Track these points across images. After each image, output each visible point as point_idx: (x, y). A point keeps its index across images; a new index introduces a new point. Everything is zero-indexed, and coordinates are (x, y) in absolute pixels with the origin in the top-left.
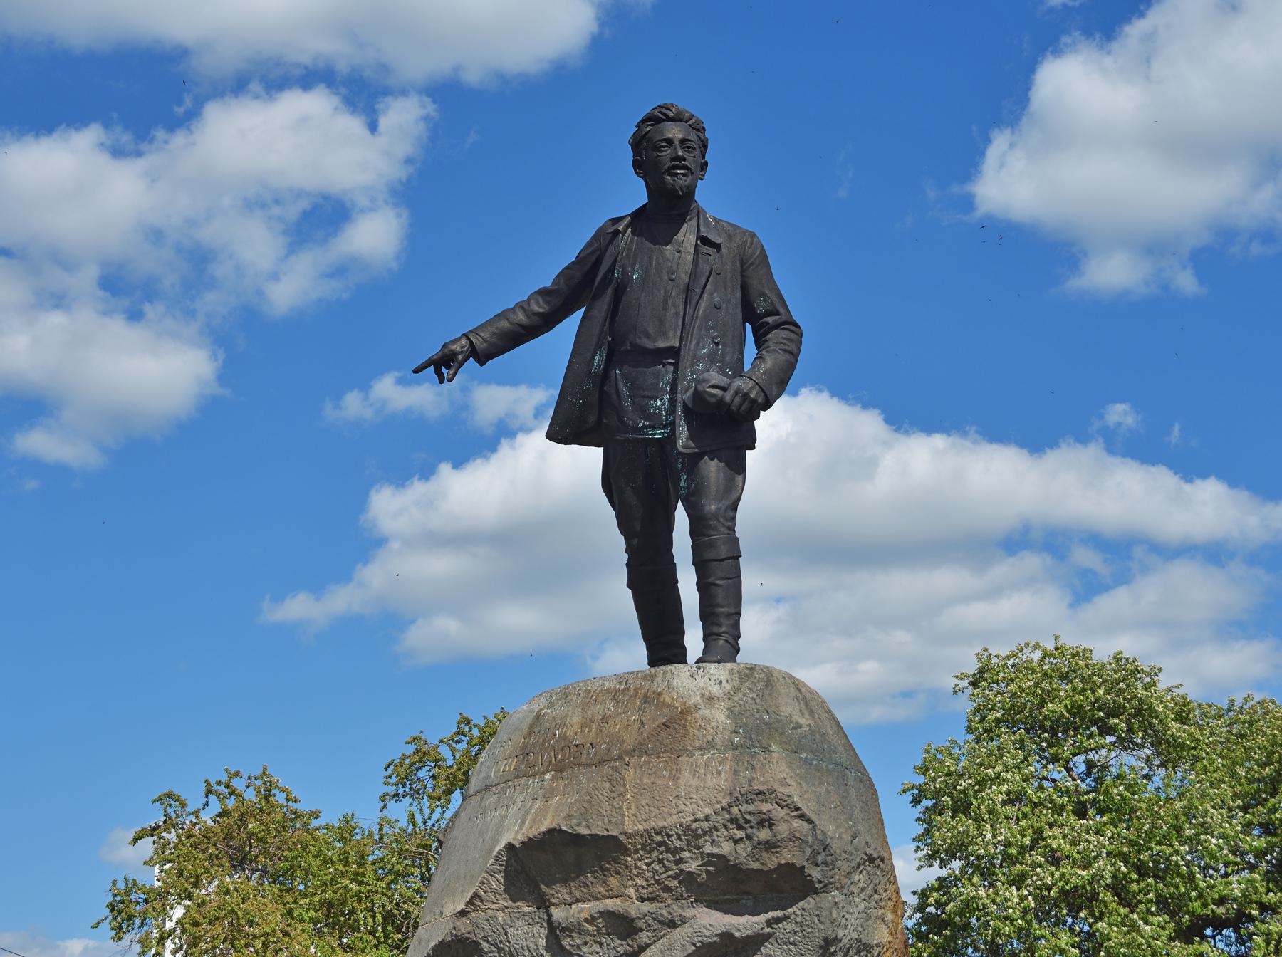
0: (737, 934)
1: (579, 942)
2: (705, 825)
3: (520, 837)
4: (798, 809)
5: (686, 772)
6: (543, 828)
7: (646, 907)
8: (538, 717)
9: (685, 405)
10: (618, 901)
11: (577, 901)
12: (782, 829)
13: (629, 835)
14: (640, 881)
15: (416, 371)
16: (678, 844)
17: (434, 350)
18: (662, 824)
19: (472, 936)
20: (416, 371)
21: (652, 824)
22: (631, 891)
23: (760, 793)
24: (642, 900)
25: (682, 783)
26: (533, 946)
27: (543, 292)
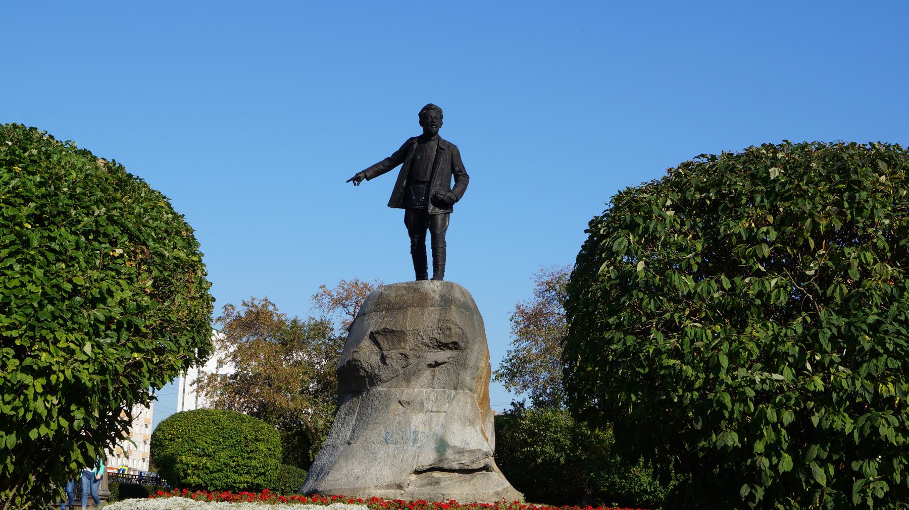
7: (412, 352)
12: (453, 331)
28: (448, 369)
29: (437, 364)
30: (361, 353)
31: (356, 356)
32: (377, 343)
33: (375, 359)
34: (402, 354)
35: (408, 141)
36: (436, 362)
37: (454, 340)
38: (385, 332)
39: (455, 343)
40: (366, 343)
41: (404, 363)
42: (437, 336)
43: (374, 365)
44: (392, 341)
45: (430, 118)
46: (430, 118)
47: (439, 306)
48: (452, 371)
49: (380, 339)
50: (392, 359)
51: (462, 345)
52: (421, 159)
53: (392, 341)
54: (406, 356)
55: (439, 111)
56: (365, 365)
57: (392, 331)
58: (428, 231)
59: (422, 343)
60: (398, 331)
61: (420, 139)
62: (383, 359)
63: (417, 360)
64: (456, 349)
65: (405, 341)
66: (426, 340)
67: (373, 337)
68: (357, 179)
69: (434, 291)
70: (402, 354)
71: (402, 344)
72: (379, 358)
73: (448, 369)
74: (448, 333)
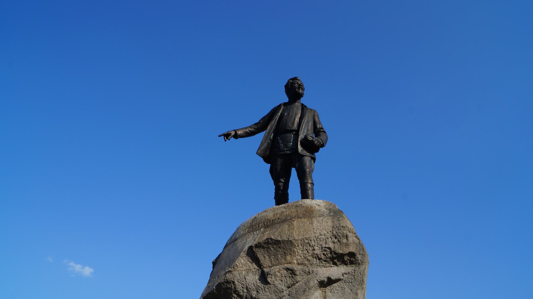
0: (332, 278)
1: (274, 279)
2: (323, 237)
3: (255, 243)
4: (355, 233)
5: (315, 222)
6: (265, 238)
7: (300, 267)
8: (255, 218)
9: (301, 141)
10: (290, 265)
11: (274, 265)
12: (350, 239)
13: (296, 240)
14: (298, 257)
15: (219, 136)
16: (313, 243)
17: (225, 132)
18: (308, 236)
19: (233, 280)
20: (219, 136)
21: (305, 236)
22: (295, 261)
23: (343, 227)
24: (299, 264)
25: (315, 225)
26: (255, 283)
27: (256, 124)
28: (343, 289)
29: (330, 282)
30: (236, 273)
31: (229, 276)
32: (255, 260)
33: (253, 279)
34: (287, 269)
35: (273, 110)
36: (329, 279)
37: (352, 249)
38: (270, 244)
39: (352, 255)
40: (243, 262)
41: (290, 281)
42: (331, 245)
43: (251, 286)
44: (276, 255)
45: (294, 90)
46: (294, 90)
47: (329, 215)
48: (347, 290)
49: (260, 254)
50: (275, 276)
51: (359, 257)
52: (288, 114)
53: (276, 255)
54: (292, 272)
55: (301, 86)
56: (239, 287)
57: (277, 243)
58: (294, 171)
59: (313, 256)
60: (284, 241)
61: (285, 104)
62: (264, 278)
63: (306, 277)
64: (352, 263)
65: (292, 253)
66: (318, 251)
67: (252, 254)
68: (227, 136)
69: (319, 205)
70: (287, 269)
71: (288, 258)
72: (257, 277)
73: (343, 289)
74: (345, 241)
